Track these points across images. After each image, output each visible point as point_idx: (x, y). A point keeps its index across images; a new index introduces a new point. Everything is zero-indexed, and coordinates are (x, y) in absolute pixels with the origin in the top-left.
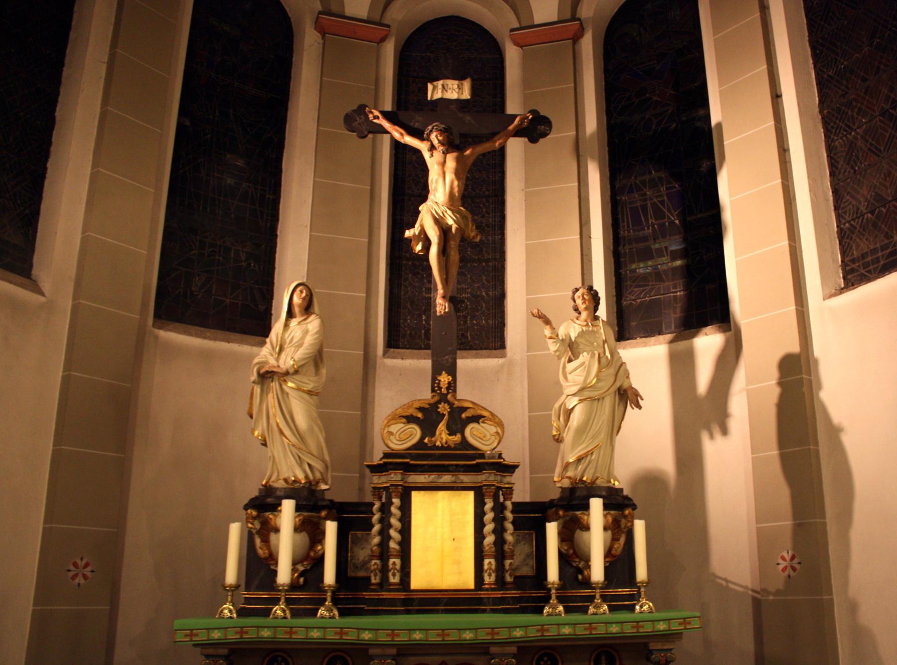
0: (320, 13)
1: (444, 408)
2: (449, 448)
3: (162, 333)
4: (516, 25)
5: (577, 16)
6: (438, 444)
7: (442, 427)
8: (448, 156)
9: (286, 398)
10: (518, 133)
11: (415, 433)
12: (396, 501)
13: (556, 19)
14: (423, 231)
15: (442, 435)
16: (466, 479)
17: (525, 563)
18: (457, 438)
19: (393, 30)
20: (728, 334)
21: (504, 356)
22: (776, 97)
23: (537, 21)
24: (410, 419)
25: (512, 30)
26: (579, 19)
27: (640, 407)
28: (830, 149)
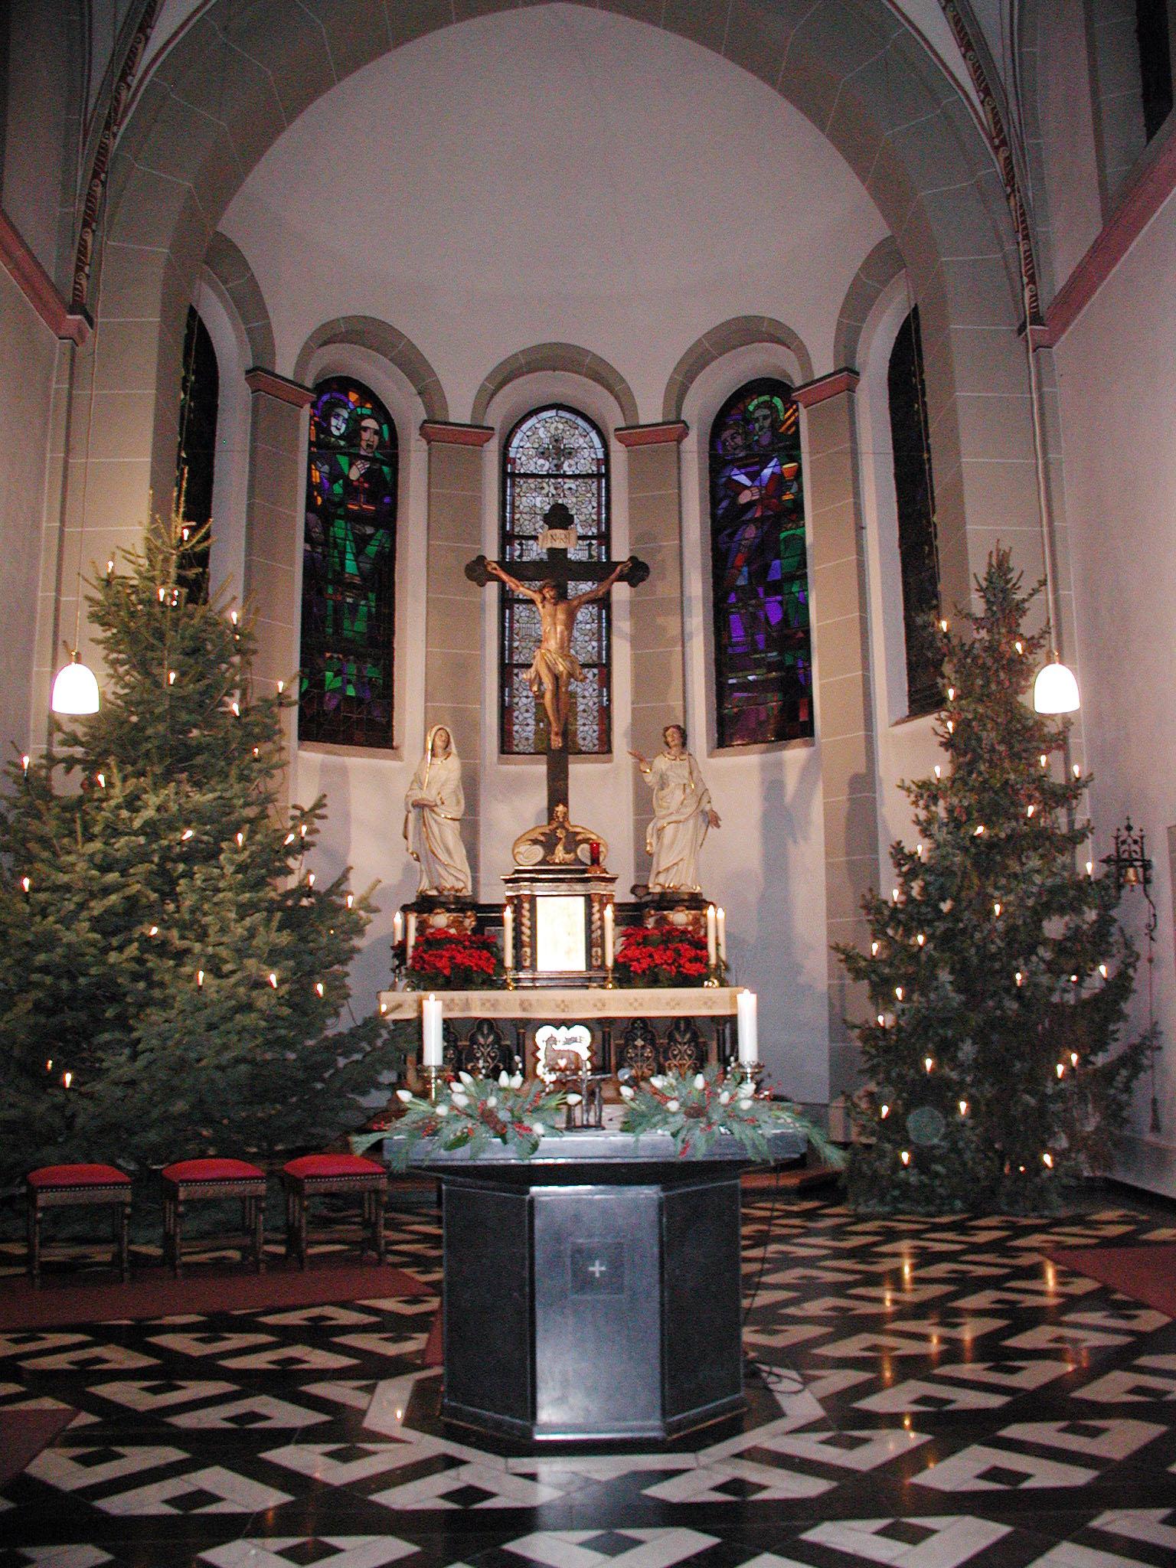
0: (425, 422)
1: (560, 833)
2: (566, 864)
3: (302, 754)
4: (623, 425)
5: (682, 418)
6: (557, 861)
7: (560, 848)
8: (559, 607)
9: (837, 1003)
10: (620, 579)
11: (539, 852)
12: (526, 906)
13: (660, 420)
14: (538, 674)
15: (560, 854)
16: (579, 888)
17: (681, 1136)
18: (571, 856)
19: (497, 431)
20: (812, 749)
21: (610, 761)
22: (860, 528)
23: (642, 422)
24: (535, 842)
25: (617, 430)
26: (683, 422)
27: (718, 826)
28: (906, 584)
